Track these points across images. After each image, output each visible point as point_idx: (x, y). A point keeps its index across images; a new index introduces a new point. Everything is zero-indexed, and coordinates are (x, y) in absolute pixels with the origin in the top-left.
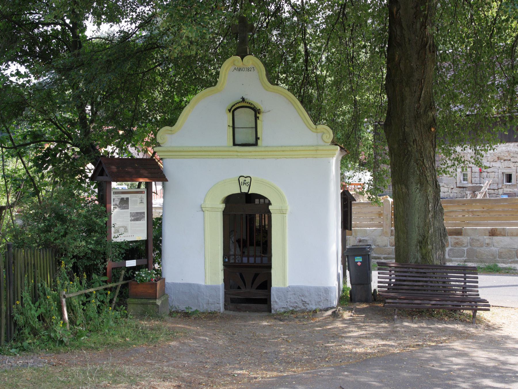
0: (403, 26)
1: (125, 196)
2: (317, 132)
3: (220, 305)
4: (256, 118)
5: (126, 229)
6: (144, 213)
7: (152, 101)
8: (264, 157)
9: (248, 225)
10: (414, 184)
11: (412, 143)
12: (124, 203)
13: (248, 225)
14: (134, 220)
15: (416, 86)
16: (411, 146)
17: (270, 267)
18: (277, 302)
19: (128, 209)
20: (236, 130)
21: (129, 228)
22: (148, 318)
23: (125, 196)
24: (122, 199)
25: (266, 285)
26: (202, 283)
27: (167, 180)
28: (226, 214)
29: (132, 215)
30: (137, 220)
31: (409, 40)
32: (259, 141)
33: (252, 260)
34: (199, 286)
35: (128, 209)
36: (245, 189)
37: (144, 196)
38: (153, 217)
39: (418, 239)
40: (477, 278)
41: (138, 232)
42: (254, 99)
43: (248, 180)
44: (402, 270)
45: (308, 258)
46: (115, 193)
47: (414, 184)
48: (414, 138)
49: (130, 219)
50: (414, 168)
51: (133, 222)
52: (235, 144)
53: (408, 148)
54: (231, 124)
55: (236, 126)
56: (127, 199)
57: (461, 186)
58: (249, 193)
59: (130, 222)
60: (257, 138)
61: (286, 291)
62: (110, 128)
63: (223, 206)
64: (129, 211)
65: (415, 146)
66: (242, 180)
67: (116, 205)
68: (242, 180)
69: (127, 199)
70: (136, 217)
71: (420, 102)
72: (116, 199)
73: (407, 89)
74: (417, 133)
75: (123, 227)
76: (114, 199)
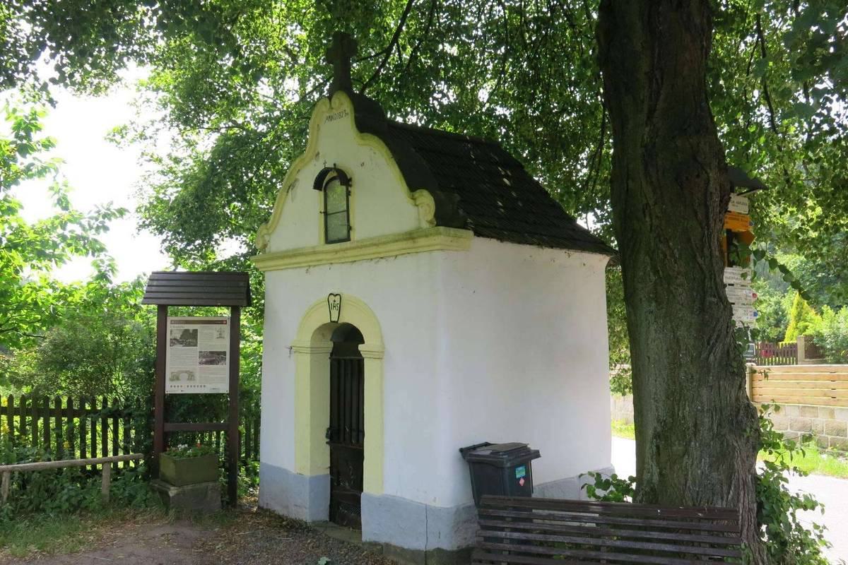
1: (191, 327)
4: (348, 193)
5: (191, 376)
6: (224, 353)
7: (563, 19)
8: (431, 248)
10: (645, 304)
14: (207, 363)
19: (196, 345)
21: (197, 375)
22: (178, 519)
24: (187, 331)
29: (202, 355)
30: (211, 362)
32: (352, 233)
35: (196, 345)
38: (632, 396)
41: (215, 381)
47: (645, 304)
48: (645, 201)
49: (198, 360)
51: (202, 366)
52: (328, 241)
55: (345, 213)
56: (196, 331)
57: (218, 326)
59: (199, 366)
60: (350, 228)
64: (198, 349)
65: (648, 219)
69: (196, 331)
70: (212, 358)
75: (186, 372)
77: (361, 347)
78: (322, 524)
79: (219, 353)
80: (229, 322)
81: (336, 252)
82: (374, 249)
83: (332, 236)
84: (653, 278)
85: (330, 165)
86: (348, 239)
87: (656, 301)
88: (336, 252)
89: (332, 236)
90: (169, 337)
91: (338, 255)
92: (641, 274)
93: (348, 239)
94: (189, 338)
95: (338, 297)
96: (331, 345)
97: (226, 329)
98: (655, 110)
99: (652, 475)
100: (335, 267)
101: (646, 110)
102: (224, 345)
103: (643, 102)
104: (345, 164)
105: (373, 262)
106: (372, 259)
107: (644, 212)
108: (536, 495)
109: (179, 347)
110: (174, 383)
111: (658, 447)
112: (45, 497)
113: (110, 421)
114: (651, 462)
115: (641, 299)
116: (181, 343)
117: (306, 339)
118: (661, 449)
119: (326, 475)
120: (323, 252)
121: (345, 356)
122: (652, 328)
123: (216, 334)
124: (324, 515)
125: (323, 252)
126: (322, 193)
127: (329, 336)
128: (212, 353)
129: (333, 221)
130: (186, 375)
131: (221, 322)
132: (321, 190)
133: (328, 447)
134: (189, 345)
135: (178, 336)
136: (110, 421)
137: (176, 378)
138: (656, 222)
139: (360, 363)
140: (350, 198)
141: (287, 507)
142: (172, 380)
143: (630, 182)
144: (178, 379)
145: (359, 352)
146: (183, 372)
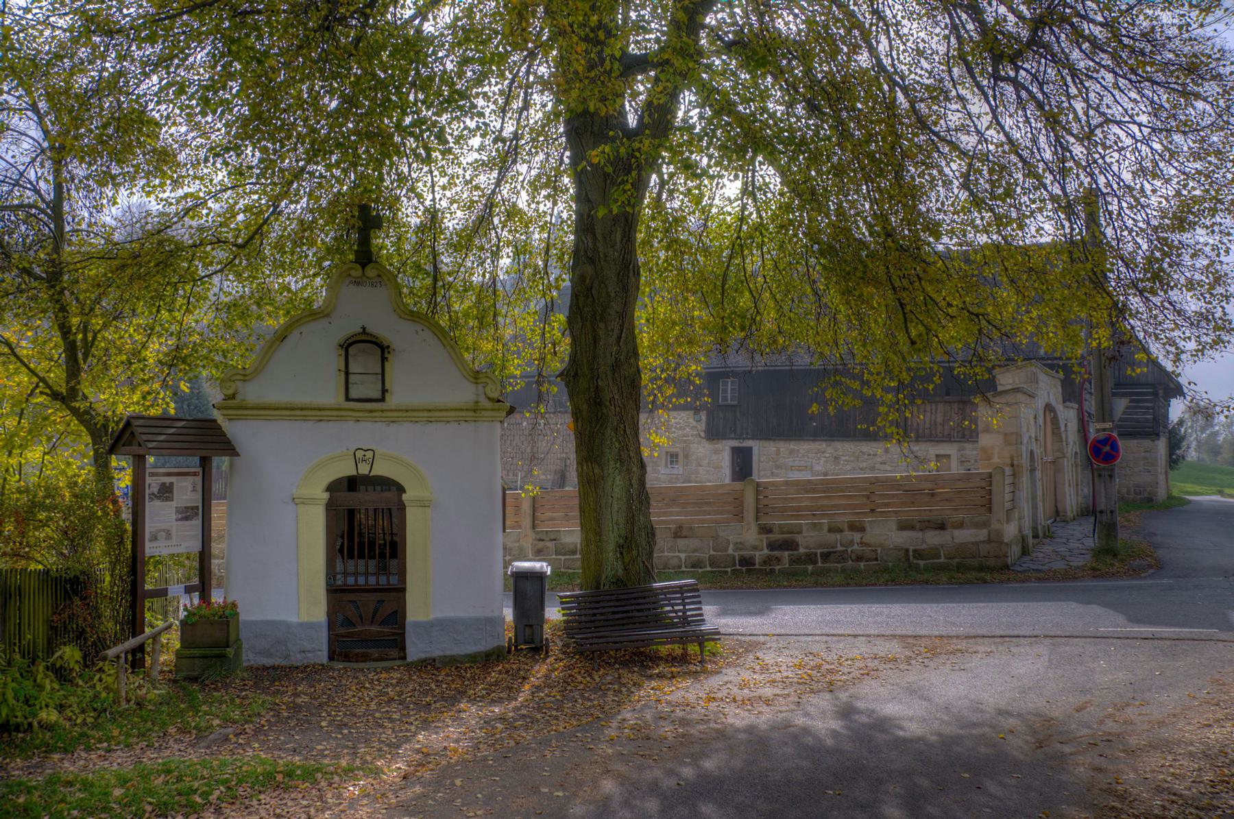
1: (167, 480)
3: (322, 656)
4: (384, 360)
5: (168, 535)
9: (367, 531)
10: (612, 462)
12: (166, 492)
13: (367, 531)
14: (181, 519)
17: (402, 591)
20: (352, 378)
21: (174, 534)
23: (167, 480)
24: (163, 484)
25: (397, 617)
26: (294, 619)
27: (238, 455)
28: (331, 507)
29: (178, 510)
30: (186, 519)
32: (387, 395)
33: (372, 580)
34: (287, 625)
37: (199, 479)
40: (700, 609)
42: (381, 330)
43: (369, 454)
44: (593, 605)
45: (456, 580)
46: (152, 474)
52: (348, 399)
54: (343, 368)
55: (351, 370)
56: (172, 484)
59: (175, 523)
60: (384, 391)
62: (120, 762)
63: (326, 496)
64: (174, 504)
66: (359, 454)
68: (359, 454)
69: (172, 484)
73: (602, 325)
79: (192, 508)
81: (371, 411)
82: (426, 414)
83: (354, 393)
86: (383, 399)
88: (371, 411)
89: (354, 393)
93: (383, 399)
105: (418, 425)
109: (157, 503)
110: (154, 544)
112: (4, 4)
116: (158, 498)
122: (618, 478)
126: (343, 353)
135: (156, 490)
137: (154, 538)
139: (402, 508)
141: (287, 657)
142: (150, 541)
144: (156, 539)
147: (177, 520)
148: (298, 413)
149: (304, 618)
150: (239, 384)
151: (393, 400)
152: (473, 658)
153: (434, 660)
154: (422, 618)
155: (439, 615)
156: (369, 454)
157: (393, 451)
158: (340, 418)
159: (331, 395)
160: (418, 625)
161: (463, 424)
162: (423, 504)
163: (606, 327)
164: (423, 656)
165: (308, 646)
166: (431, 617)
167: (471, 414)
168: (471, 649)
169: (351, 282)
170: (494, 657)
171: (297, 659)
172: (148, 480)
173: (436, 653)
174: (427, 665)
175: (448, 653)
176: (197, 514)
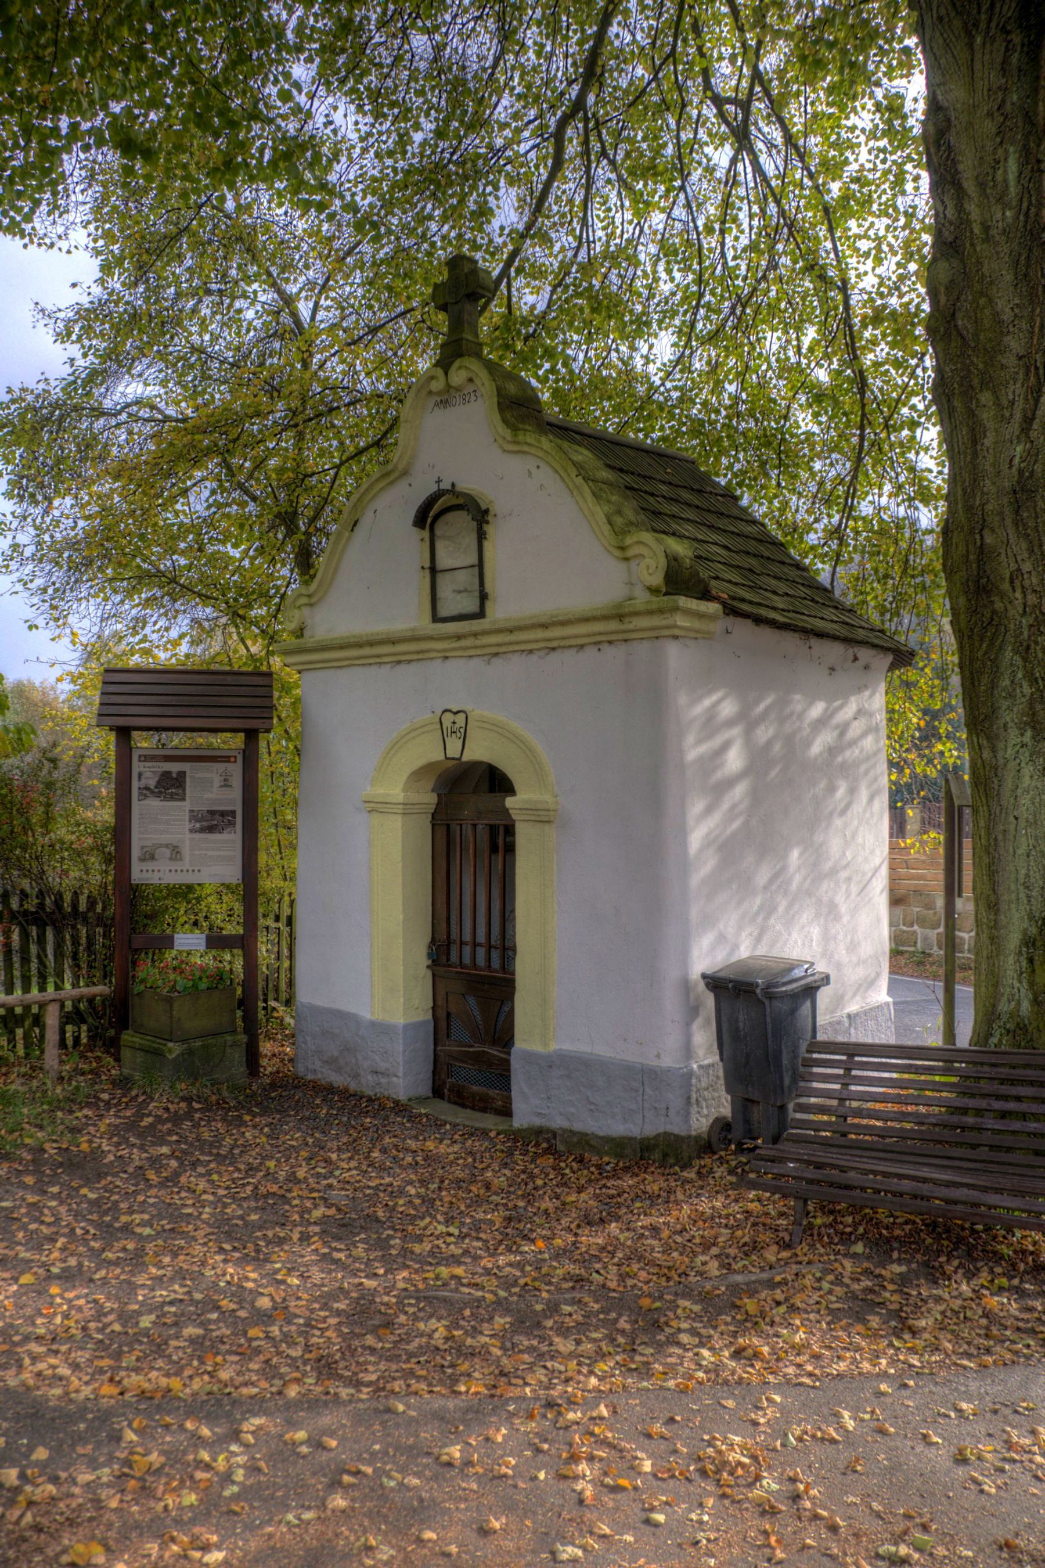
0: (965, 185)
1: (174, 767)
2: (626, 559)
4: (481, 536)
5: (176, 853)
11: (1006, 586)
14: (202, 830)
15: (1015, 381)
16: (1002, 595)
18: (526, 1112)
21: (186, 852)
23: (174, 767)
24: (166, 774)
29: (194, 816)
30: (211, 829)
31: (986, 228)
32: (488, 605)
36: (454, 748)
39: (1025, 932)
43: (460, 719)
48: (1013, 566)
49: (188, 826)
50: (1014, 673)
51: (198, 836)
52: (436, 619)
53: (992, 603)
54: (427, 565)
56: (182, 774)
57: (221, 766)
58: (465, 759)
60: (483, 597)
61: (574, 1068)
64: (187, 805)
65: (1018, 594)
66: (448, 719)
67: (147, 788)
69: (182, 774)
70: (212, 822)
71: (1033, 435)
72: (148, 774)
73: (986, 397)
74: (1024, 545)
75: (167, 846)
76: (140, 775)
77: (510, 802)
78: (421, 1100)
80: (240, 758)
81: (459, 637)
82: (540, 634)
83: (443, 612)
84: (1027, 690)
85: (445, 485)
87: (1034, 728)
88: (459, 637)
89: (443, 612)
90: (135, 785)
91: (463, 643)
92: (1007, 682)
93: (481, 614)
94: (171, 786)
95: (462, 716)
96: (433, 799)
97: (236, 770)
98: (1033, 418)
99: (1019, 1004)
100: (452, 664)
101: (1018, 416)
102: (233, 798)
103: (1012, 403)
104: (470, 483)
105: (534, 658)
106: (531, 651)
107: (1012, 582)
108: (821, 1037)
109: (154, 803)
110: (149, 865)
111: (1031, 961)
113: (34, 931)
114: (1017, 985)
115: (1005, 725)
116: (157, 795)
117: (394, 789)
118: (1037, 963)
119: (423, 1023)
120: (431, 638)
121: (471, 821)
122: (1027, 771)
123: (217, 781)
124: (424, 1089)
125: (431, 638)
126: (426, 534)
127: (430, 785)
128: (212, 813)
129: (446, 587)
130: (167, 852)
131: (226, 759)
132: (423, 527)
133: (429, 974)
134: (172, 797)
135: (152, 783)
136: (34, 931)
137: (149, 856)
138: (1032, 599)
140: (487, 544)
141: (356, 1076)
142: (142, 860)
143: (986, 532)
144: (152, 858)
145: (506, 811)
146: (161, 846)
147: (191, 831)
148: (367, 651)
149: (378, 1016)
150: (306, 611)
151: (499, 612)
152: (619, 1146)
153: (555, 1134)
154: (537, 1048)
155: (567, 1046)
156: (460, 719)
157: (505, 711)
158: (421, 657)
159: (407, 613)
160: (530, 1057)
161: (605, 647)
162: (543, 817)
163: (998, 404)
164: (538, 1122)
165: (383, 1066)
166: (553, 1047)
167: (613, 625)
168: (618, 1128)
169: (436, 404)
170: (657, 1155)
171: (367, 1084)
172: (137, 767)
173: (558, 1122)
174: (544, 1142)
175: (578, 1126)
176: (232, 824)
